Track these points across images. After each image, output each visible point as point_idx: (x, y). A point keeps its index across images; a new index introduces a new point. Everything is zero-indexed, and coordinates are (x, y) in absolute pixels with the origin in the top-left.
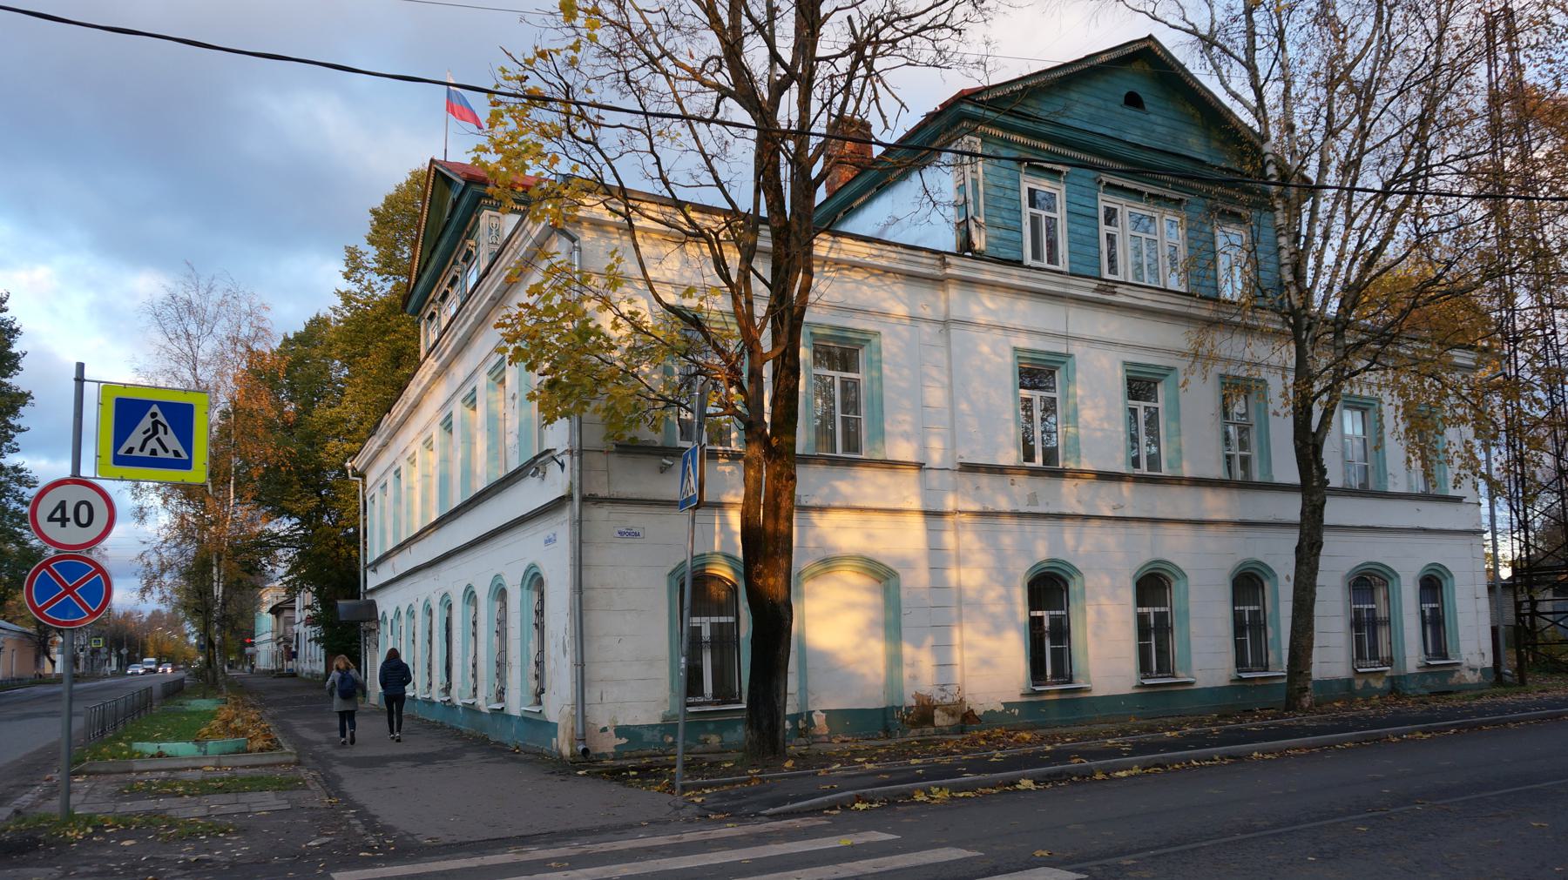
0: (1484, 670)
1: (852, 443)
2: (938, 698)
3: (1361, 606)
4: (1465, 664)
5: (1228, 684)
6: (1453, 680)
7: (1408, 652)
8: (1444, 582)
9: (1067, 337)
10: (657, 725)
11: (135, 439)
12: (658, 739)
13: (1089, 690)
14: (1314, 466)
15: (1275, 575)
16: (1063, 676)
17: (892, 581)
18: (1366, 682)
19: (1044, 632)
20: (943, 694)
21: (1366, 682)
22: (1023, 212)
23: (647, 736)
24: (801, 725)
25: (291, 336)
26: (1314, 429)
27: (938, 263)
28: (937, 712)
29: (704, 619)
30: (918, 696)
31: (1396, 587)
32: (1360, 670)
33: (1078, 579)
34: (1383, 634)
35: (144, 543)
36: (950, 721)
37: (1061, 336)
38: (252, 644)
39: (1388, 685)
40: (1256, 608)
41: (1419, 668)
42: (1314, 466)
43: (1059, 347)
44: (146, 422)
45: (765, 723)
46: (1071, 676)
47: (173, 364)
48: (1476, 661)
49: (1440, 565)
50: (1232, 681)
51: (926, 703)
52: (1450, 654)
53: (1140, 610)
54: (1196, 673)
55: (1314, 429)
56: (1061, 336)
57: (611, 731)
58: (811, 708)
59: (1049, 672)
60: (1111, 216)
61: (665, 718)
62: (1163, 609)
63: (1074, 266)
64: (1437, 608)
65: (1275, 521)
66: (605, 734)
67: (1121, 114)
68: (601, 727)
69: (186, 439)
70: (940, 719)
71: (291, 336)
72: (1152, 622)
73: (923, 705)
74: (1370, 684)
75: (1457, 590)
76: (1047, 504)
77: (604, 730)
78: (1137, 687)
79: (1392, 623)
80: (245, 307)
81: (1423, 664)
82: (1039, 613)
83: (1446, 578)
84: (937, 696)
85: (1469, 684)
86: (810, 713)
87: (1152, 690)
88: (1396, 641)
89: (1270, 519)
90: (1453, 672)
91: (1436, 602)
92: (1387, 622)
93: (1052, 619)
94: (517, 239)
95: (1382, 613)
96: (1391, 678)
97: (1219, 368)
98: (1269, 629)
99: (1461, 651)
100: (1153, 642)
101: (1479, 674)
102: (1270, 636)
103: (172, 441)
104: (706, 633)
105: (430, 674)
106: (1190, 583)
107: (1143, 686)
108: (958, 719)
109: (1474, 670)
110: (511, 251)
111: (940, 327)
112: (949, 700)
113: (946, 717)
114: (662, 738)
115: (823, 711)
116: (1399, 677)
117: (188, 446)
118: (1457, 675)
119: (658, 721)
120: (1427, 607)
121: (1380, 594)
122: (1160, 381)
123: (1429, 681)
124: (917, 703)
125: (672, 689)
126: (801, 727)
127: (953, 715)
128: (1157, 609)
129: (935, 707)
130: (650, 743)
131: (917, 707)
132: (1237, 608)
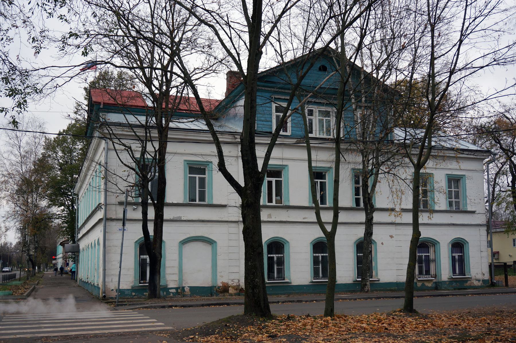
0: (484, 281)
1: (202, 198)
2: (231, 284)
3: (423, 254)
4: (473, 278)
5: (353, 282)
7: (443, 272)
8: (463, 246)
9: (283, 159)
10: (129, 289)
12: (130, 294)
13: (291, 283)
14: (369, 205)
15: (376, 243)
16: (282, 277)
17: (214, 244)
19: (147, 263)
20: (233, 282)
22: (273, 114)
23: (126, 293)
24: (179, 291)
25: (62, 131)
27: (233, 137)
28: (230, 288)
30: (222, 283)
31: (438, 247)
32: (418, 279)
33: (287, 244)
34: (432, 266)
35: (3, 217)
36: (235, 292)
37: (280, 159)
38: (55, 259)
39: (434, 285)
40: (461, 254)
41: (448, 279)
42: (369, 205)
43: (285, 163)
45: (152, 288)
46: (284, 278)
47: (11, 148)
48: (480, 277)
49: (459, 238)
50: (354, 281)
51: (226, 285)
52: (466, 274)
53: (315, 255)
56: (280, 159)
57: (115, 290)
58: (184, 285)
60: (311, 113)
61: (132, 287)
63: (294, 132)
64: (462, 255)
65: (377, 222)
66: (113, 291)
67: (317, 74)
68: (111, 289)
70: (231, 291)
71: (62, 131)
72: (457, 258)
73: (225, 286)
74: (425, 285)
75: (470, 248)
76: (275, 218)
77: (113, 290)
78: (311, 282)
79: (436, 261)
80: (38, 124)
81: (450, 277)
82: (317, 255)
83: (465, 244)
84: (230, 283)
85: (475, 286)
86: (183, 288)
87: (318, 284)
88: (438, 267)
90: (468, 281)
91: (462, 253)
92: (434, 261)
93: (278, 258)
95: (432, 257)
96: (436, 282)
97: (352, 166)
98: (373, 262)
99: (471, 273)
100: (320, 266)
101: (481, 282)
102: (373, 265)
104: (457, 257)
105: (448, 295)
106: (219, 250)
107: (313, 282)
108: (238, 291)
109: (479, 280)
111: (235, 158)
112: (235, 284)
113: (234, 290)
114: (131, 293)
115: (188, 287)
116: (439, 282)
118: (469, 282)
119: (130, 288)
120: (456, 255)
121: (432, 250)
122: (327, 172)
123: (454, 284)
124: (223, 285)
125: (135, 278)
126: (179, 291)
127: (236, 290)
128: (322, 255)
129: (229, 287)
130: (127, 295)
131: (223, 286)
132: (358, 255)
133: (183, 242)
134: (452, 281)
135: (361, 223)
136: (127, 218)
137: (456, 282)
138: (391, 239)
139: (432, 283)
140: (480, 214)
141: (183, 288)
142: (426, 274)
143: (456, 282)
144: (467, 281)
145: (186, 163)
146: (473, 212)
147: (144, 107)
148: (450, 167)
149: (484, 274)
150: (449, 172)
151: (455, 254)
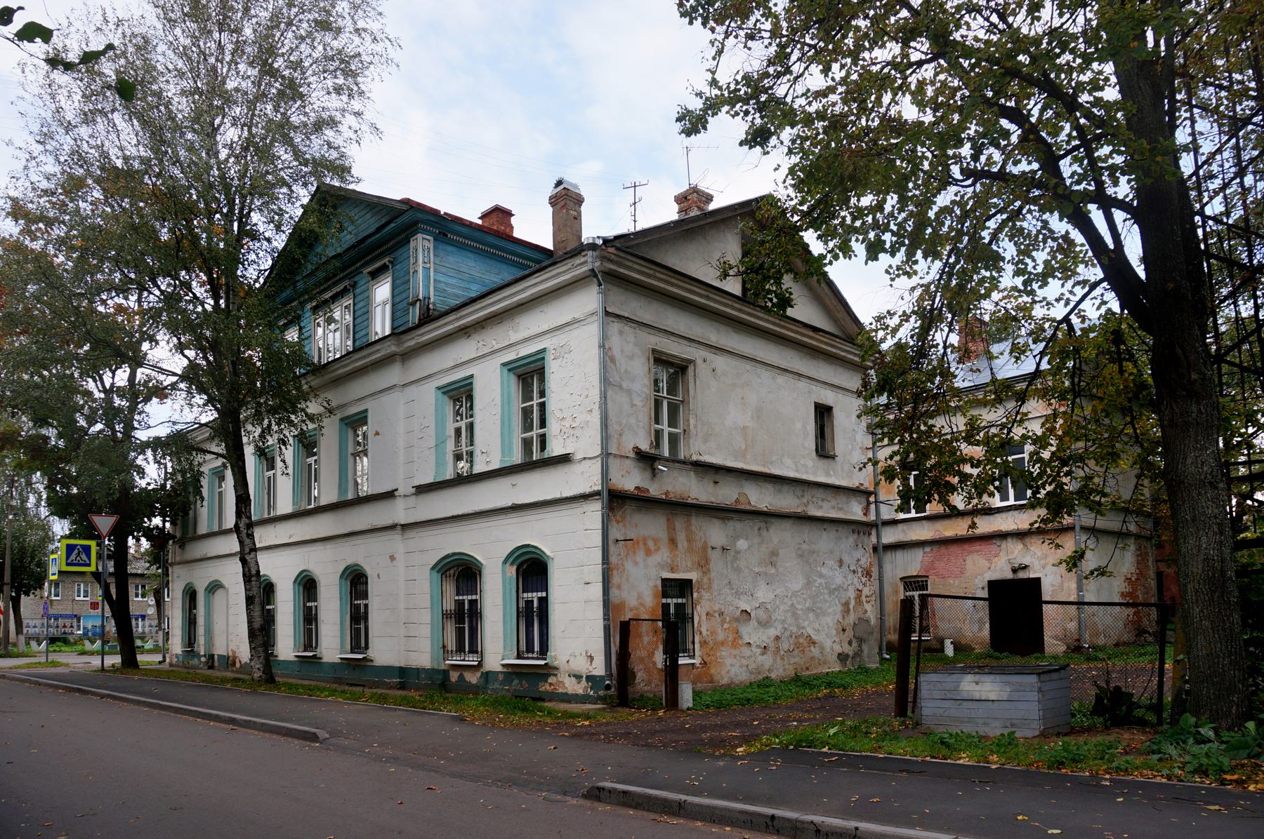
6: (544, 687)
11: (73, 557)
18: (461, 675)
21: (461, 675)
26: (1111, 246)
29: (535, 594)
44: (76, 551)
48: (582, 666)
54: (324, 652)
55: (1111, 246)
59: (467, 649)
62: (474, 597)
69: (89, 557)
89: (369, 527)
94: (640, 265)
97: (339, 416)
100: (466, 626)
103: (84, 557)
109: (578, 677)
110: (652, 272)
117: (90, 559)
118: (551, 680)
133: (511, 559)
134: (513, 672)
135: (584, 497)
136: (259, 557)
137: (519, 675)
138: (370, 571)
139: (478, 674)
140: (588, 461)
141: (213, 655)
142: (470, 652)
143: (519, 675)
144: (545, 677)
145: (505, 371)
146: (565, 459)
147: (393, 305)
148: (514, 337)
149: (591, 658)
150: (510, 356)
151: (530, 595)
